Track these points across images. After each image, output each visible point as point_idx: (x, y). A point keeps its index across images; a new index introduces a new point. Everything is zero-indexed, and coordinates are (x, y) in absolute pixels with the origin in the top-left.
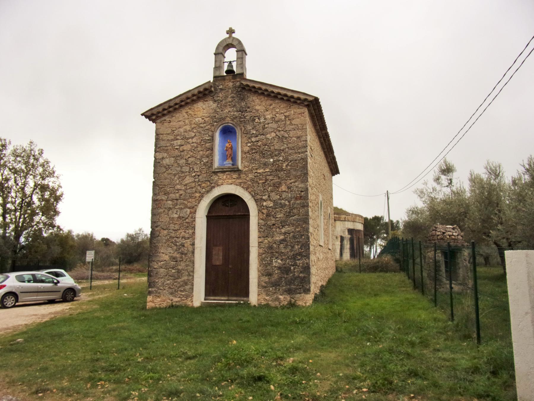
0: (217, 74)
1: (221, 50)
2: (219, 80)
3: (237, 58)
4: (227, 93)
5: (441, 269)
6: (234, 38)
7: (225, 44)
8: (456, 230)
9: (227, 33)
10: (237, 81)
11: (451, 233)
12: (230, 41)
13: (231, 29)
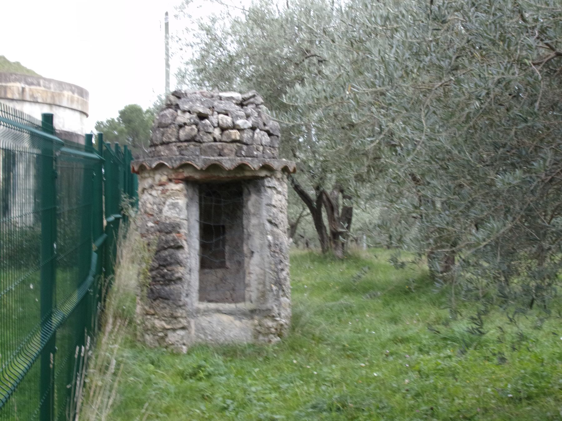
5: (181, 255)
8: (250, 109)
11: (227, 120)
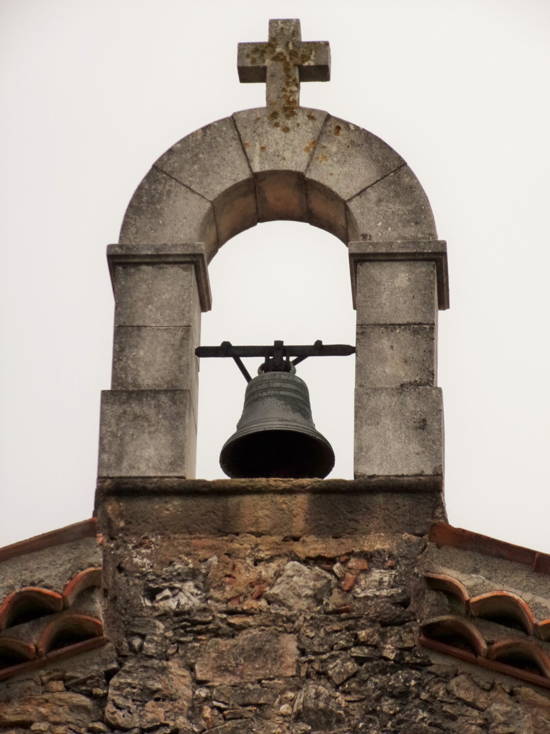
0: (147, 460)
1: (182, 222)
2: (163, 528)
3: (363, 329)
4: (252, 671)
6: (329, 126)
7: (233, 173)
9: (247, 75)
10: (370, 558)
12: (288, 152)
13: (285, 31)
